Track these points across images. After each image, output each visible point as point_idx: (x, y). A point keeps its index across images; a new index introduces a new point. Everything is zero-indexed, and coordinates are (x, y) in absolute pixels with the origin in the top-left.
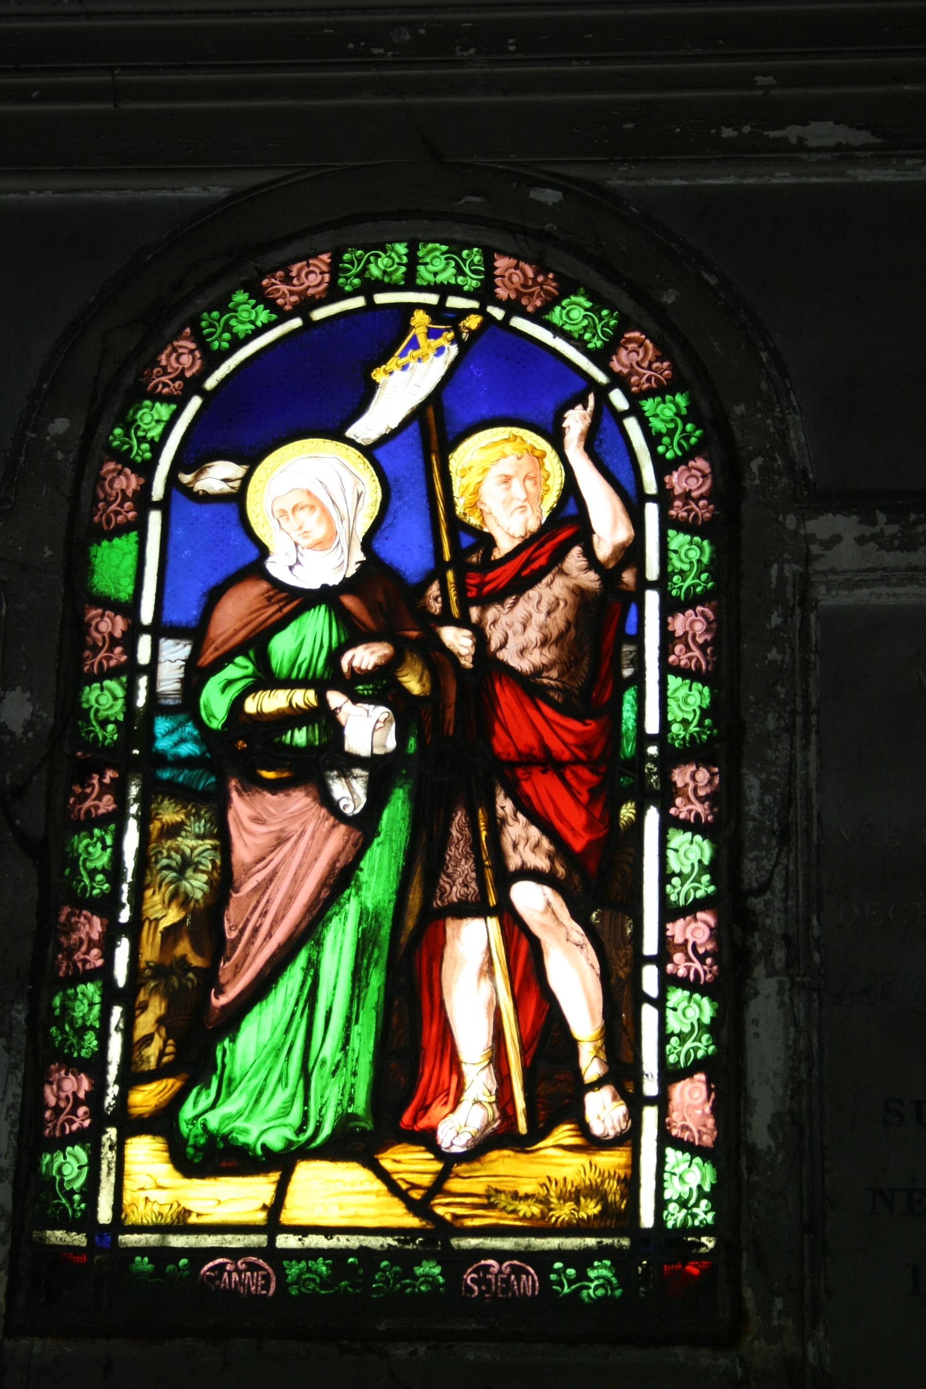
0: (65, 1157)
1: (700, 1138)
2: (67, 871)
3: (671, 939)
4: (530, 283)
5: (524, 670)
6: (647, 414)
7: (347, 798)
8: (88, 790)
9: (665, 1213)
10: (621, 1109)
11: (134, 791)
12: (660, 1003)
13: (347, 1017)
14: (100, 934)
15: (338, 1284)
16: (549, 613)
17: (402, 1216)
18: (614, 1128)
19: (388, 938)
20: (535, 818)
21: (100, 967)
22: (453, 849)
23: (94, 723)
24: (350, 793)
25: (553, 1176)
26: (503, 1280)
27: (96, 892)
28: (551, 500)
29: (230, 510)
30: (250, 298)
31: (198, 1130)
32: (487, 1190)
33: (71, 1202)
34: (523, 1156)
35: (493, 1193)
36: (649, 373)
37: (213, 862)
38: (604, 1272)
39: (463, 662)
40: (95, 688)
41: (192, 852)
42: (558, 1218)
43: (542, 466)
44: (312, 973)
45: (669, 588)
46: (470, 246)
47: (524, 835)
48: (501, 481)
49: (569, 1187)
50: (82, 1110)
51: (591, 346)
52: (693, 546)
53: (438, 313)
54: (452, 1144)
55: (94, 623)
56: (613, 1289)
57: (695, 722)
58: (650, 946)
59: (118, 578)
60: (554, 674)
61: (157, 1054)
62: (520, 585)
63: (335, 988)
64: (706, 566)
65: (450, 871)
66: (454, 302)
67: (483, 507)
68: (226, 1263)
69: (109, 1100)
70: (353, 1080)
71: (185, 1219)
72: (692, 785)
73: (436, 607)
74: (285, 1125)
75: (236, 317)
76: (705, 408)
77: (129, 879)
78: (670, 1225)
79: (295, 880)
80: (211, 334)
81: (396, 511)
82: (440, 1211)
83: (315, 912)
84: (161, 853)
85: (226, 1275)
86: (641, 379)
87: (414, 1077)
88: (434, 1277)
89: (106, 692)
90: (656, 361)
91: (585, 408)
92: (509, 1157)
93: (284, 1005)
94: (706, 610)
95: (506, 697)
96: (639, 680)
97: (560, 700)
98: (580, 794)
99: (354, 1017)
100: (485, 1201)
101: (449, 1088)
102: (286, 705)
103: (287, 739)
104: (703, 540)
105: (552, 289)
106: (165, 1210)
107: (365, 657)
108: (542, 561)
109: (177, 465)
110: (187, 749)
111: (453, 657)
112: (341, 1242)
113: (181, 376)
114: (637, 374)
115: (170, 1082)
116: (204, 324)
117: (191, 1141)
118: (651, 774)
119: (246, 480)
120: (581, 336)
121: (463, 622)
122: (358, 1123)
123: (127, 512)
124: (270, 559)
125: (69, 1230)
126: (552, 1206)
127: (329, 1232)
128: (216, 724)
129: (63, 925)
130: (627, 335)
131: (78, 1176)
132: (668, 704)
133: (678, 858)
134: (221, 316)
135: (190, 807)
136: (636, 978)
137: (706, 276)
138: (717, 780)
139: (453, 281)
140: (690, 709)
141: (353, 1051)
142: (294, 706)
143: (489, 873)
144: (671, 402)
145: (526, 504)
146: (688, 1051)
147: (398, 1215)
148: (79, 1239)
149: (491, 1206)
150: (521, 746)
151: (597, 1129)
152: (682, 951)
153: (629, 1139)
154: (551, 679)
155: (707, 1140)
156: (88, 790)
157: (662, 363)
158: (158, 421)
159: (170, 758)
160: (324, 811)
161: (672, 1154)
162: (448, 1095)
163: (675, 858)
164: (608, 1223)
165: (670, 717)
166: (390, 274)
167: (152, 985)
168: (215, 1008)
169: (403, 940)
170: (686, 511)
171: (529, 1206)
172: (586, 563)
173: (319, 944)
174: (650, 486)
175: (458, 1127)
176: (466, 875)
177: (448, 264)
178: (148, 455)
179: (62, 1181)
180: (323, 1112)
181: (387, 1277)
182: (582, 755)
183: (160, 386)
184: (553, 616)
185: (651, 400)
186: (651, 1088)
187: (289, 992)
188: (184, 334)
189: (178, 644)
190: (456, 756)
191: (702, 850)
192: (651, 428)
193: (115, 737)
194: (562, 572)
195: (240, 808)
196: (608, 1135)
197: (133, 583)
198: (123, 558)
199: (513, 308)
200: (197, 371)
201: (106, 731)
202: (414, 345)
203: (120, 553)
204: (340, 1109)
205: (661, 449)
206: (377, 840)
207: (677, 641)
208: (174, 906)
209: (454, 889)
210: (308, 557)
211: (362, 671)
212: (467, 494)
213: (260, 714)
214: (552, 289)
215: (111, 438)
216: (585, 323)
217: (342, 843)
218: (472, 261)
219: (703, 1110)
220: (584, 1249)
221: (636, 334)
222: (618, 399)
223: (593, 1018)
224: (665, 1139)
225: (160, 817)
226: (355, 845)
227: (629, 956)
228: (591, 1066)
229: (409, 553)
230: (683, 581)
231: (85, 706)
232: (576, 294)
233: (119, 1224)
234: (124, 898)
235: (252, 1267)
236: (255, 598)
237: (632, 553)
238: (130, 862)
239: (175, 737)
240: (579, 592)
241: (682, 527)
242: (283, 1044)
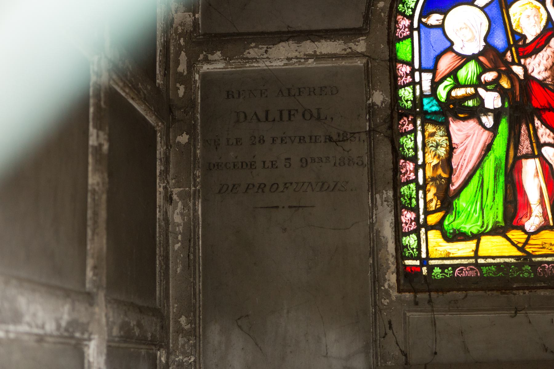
2: (401, 149)
16: (547, 60)
24: (488, 121)
28: (543, 23)
29: (438, 32)
33: (413, 252)
37: (446, 144)
43: (539, 12)
50: (413, 223)
60: (550, 80)
73: (510, 59)
79: (473, 149)
82: (528, 250)
103: (466, 104)
106: (442, 253)
107: (489, 76)
108: (543, 43)
109: (421, 16)
110: (435, 108)
111: (517, 76)
112: (498, 261)
119: (444, 20)
121: (519, 64)
125: (413, 260)
127: (494, 258)
143: (534, 145)
147: (516, 252)
148: (417, 263)
149: (544, 248)
159: (429, 112)
160: (480, 127)
169: (509, 166)
178: (411, 13)
194: (549, 46)
195: (455, 127)
206: (498, 135)
208: (435, 158)
229: (499, 42)
233: (428, 258)
235: (471, 269)
238: (420, 145)
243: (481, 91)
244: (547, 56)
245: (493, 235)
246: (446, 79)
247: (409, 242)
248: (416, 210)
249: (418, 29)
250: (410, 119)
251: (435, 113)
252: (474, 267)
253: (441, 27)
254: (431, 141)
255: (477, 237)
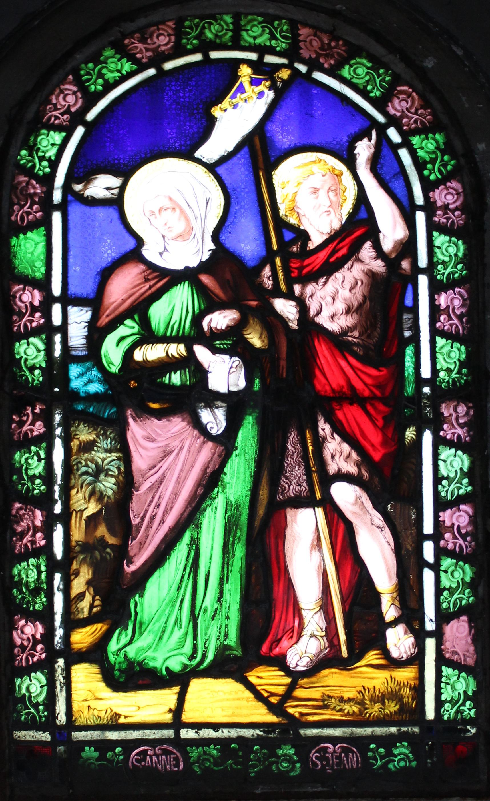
0: (31, 680)
1: (465, 660)
2: (15, 477)
3: (442, 523)
4: (326, 47)
5: (335, 331)
6: (415, 147)
7: (212, 422)
8: (25, 418)
9: (443, 710)
10: (410, 640)
11: (57, 418)
12: (436, 567)
13: (220, 578)
14: (41, 522)
15: (225, 763)
16: (351, 289)
17: (265, 715)
18: (406, 653)
19: (246, 522)
20: (347, 437)
21: (43, 546)
22: (289, 459)
23: (24, 369)
24: (215, 419)
25: (366, 686)
26: (337, 757)
27: (36, 492)
28: (348, 207)
29: (112, 213)
30: (116, 53)
31: (121, 659)
32: (322, 696)
33: (38, 711)
34: (345, 673)
35: (326, 698)
36: (416, 117)
37: (119, 469)
38: (404, 750)
39: (290, 324)
40: (24, 343)
41: (103, 463)
42: (370, 714)
43: (340, 181)
44: (194, 548)
45: (435, 274)
46: (280, 19)
47: (339, 449)
48: (312, 192)
49: (377, 693)
50: (39, 647)
51: (372, 95)
52: (451, 244)
53: (257, 67)
54: (297, 665)
55: (18, 295)
56: (410, 762)
57: (456, 371)
58: (428, 528)
59: (33, 262)
60: (356, 334)
61: (88, 606)
62: (329, 269)
63: (211, 559)
64: (461, 259)
65: (288, 474)
66: (269, 59)
67: (299, 211)
68: (148, 750)
69: (57, 640)
70: (227, 623)
71: (116, 720)
72: (454, 416)
73: (269, 284)
74: (182, 654)
75: (106, 67)
76: (458, 144)
77: (59, 482)
78: (446, 718)
79: (178, 482)
80: (88, 80)
81: (235, 213)
82: (291, 711)
83: (193, 505)
84: (81, 463)
85: (148, 757)
86: (410, 121)
87: (269, 618)
88: (290, 756)
89: (31, 346)
90: (421, 109)
91: (370, 140)
92: (336, 673)
93: (176, 570)
94: (462, 290)
95: (323, 350)
96: (415, 339)
97: (361, 353)
98: (377, 420)
99: (225, 578)
100: (321, 703)
101: (293, 627)
102: (164, 355)
103: (166, 380)
104: (458, 240)
105: (342, 52)
106: (102, 714)
107: (220, 320)
108: (344, 251)
109: (72, 177)
110: (95, 388)
111: (283, 321)
112: (225, 733)
113: (68, 111)
114: (407, 117)
115: (99, 625)
116: (82, 72)
117: (117, 667)
118: (425, 407)
119: (122, 188)
120: (365, 87)
121: (289, 295)
122: (231, 652)
123: (36, 212)
124: (144, 247)
125: (37, 730)
126: (367, 706)
127: (216, 726)
128: (114, 369)
129: (15, 516)
130: (399, 88)
131: (41, 693)
132: (436, 357)
133: (446, 466)
134: (95, 66)
135: (99, 430)
136: (420, 550)
137: (455, 48)
138: (472, 412)
139: (268, 44)
140: (452, 361)
141: (226, 602)
142: (170, 356)
143: (315, 476)
144: (432, 139)
145: (330, 209)
146: (456, 600)
147: (262, 715)
148: (46, 737)
149: (325, 707)
150: (334, 386)
151: (395, 654)
152: (450, 532)
153: (417, 660)
154: (354, 337)
155: (470, 661)
156: (25, 418)
157: (425, 110)
158: (53, 145)
159: (82, 394)
160: (196, 432)
161: (446, 671)
162: (293, 631)
163: (444, 466)
164: (404, 717)
165: (438, 367)
166: (220, 37)
167: (81, 557)
168: (128, 573)
169: (257, 523)
170: (445, 218)
171: (351, 706)
172: (375, 253)
173: (198, 527)
174: (419, 199)
175: (302, 652)
176: (299, 478)
177: (263, 31)
178: (48, 170)
179: (30, 697)
180: (207, 645)
181: (258, 756)
182: (378, 393)
183: (53, 119)
184: (353, 291)
185: (418, 137)
186: (430, 626)
187: (179, 561)
188: (68, 80)
189: (81, 310)
190: (288, 390)
191: (462, 461)
192: (418, 157)
193: (41, 379)
194: (359, 260)
195: (137, 430)
196: (402, 657)
197: (44, 265)
198: (35, 247)
199: (314, 65)
200: (80, 107)
201: (34, 375)
202: (241, 89)
203: (33, 243)
204: (218, 642)
205: (426, 173)
206: (235, 453)
207: (442, 312)
208: (92, 501)
209: (291, 487)
210: (172, 245)
211: (218, 330)
212: (286, 201)
213: (145, 361)
214: (342, 52)
215: (19, 157)
216: (367, 78)
217: (210, 455)
218: (282, 29)
219: (467, 641)
220: (389, 735)
221: (405, 88)
222: (394, 135)
223: (390, 578)
224: (441, 660)
225: (78, 437)
226: (219, 456)
227: (414, 535)
228: (390, 612)
229: (247, 243)
230: (445, 269)
231: (18, 357)
232: (360, 57)
233: (71, 724)
234: (57, 496)
235: (166, 752)
236: (136, 276)
237: (408, 247)
238: (58, 470)
239: (85, 379)
240: (371, 275)
241: (444, 230)
242: (177, 598)
243: (202, 352)
244: (353, 281)
245: (216, 677)
246: (122, 323)
247: (28, 689)
248: (46, 616)
249: (63, 207)
250: (37, 411)
251: (94, 397)
252: (171, 748)
253: (116, 203)
254: (85, 463)
255: (180, 680)
